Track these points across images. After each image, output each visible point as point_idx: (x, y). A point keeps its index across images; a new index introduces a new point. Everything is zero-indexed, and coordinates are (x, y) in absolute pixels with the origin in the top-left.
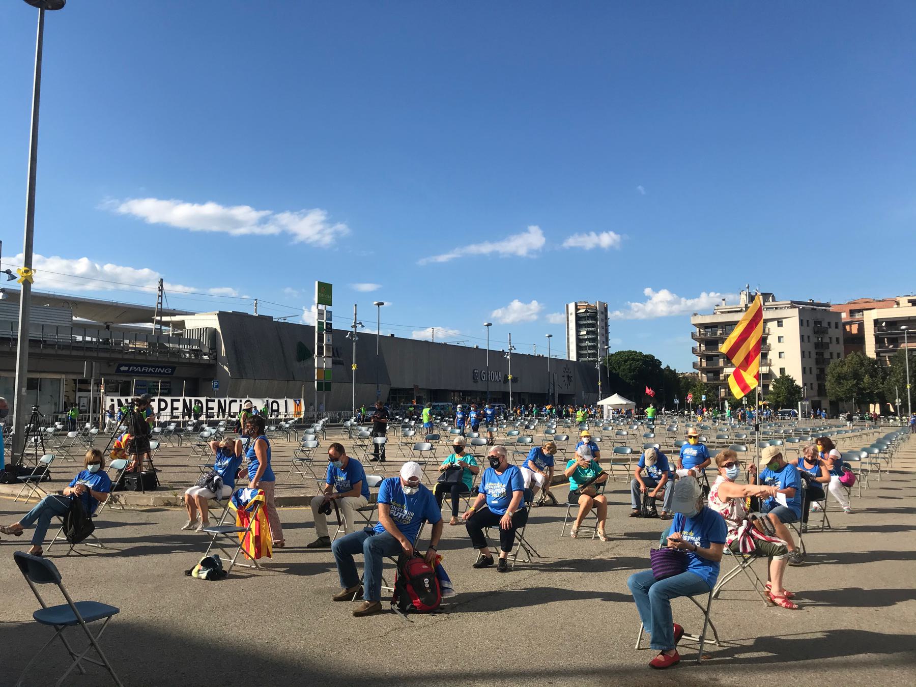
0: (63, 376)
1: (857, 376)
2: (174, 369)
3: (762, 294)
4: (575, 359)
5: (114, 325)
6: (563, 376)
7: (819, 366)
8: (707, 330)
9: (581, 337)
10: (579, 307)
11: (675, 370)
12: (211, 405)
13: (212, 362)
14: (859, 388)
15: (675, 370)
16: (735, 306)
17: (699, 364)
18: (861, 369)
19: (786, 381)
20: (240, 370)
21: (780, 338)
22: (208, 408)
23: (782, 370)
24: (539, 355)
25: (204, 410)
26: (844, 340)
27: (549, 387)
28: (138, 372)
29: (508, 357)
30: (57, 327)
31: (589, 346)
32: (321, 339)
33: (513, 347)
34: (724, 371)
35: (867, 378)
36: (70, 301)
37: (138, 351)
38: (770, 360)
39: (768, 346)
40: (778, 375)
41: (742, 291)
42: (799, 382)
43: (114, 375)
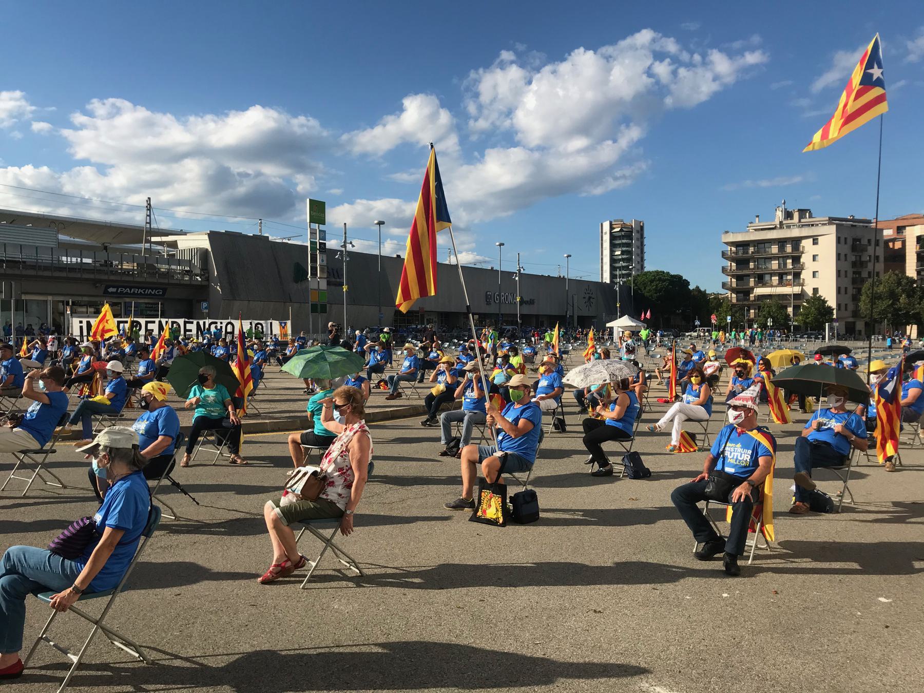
0: (50, 298)
1: (893, 296)
2: (165, 290)
3: (799, 210)
4: (608, 281)
5: (111, 246)
6: (584, 298)
7: (855, 286)
8: (738, 248)
9: (615, 257)
10: (614, 226)
11: (705, 290)
12: (189, 326)
13: (205, 283)
14: (895, 308)
15: (705, 290)
16: (769, 223)
17: (729, 283)
18: (898, 288)
19: (818, 301)
20: (232, 291)
22: (186, 330)
23: (816, 290)
24: (560, 276)
25: (182, 332)
26: (885, 257)
28: (127, 293)
29: (517, 278)
30: (37, 248)
31: (623, 267)
32: (314, 260)
34: (755, 292)
35: (903, 299)
36: (56, 220)
37: (127, 272)
38: (803, 280)
39: (802, 265)
40: (810, 293)
41: (778, 207)
42: (832, 302)
43: (101, 296)
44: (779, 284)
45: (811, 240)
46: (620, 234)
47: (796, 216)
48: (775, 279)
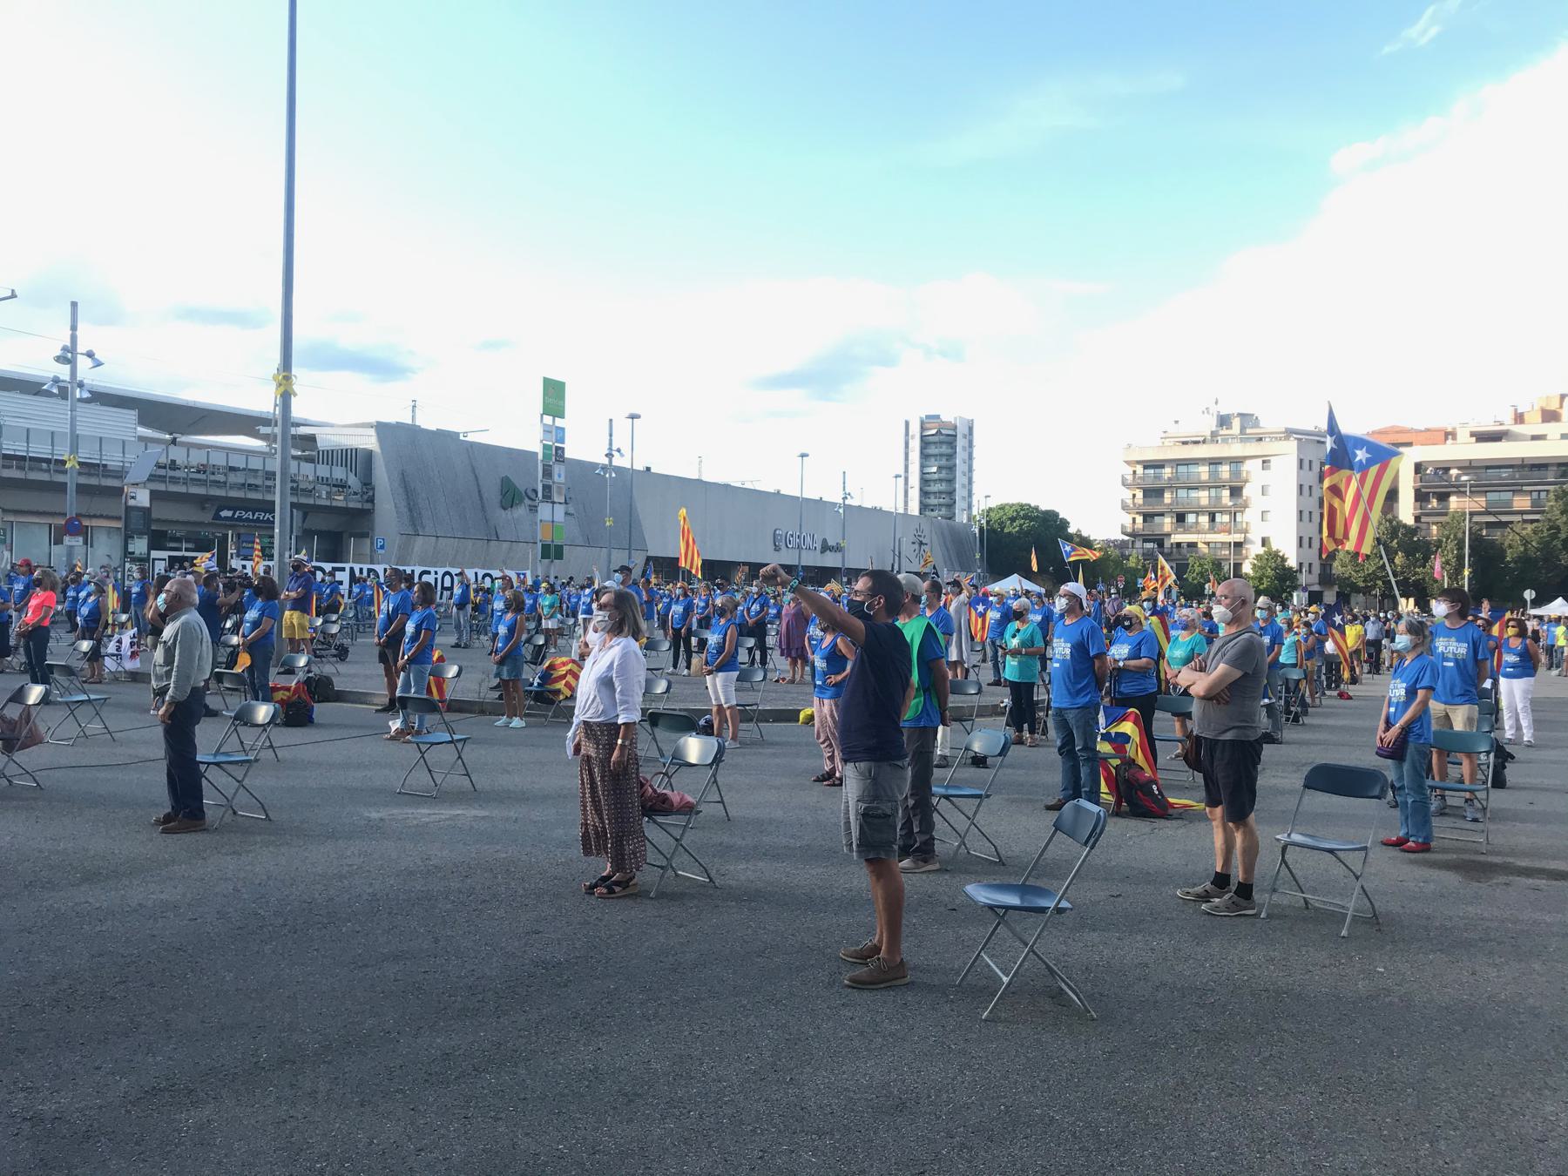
3: (1241, 415)
6: (914, 543)
10: (928, 426)
21: (1264, 491)
27: (894, 560)
28: (247, 520)
33: (849, 494)
44: (1209, 529)
45: (1260, 460)
46: (936, 439)
47: (1236, 423)
48: (1204, 519)
